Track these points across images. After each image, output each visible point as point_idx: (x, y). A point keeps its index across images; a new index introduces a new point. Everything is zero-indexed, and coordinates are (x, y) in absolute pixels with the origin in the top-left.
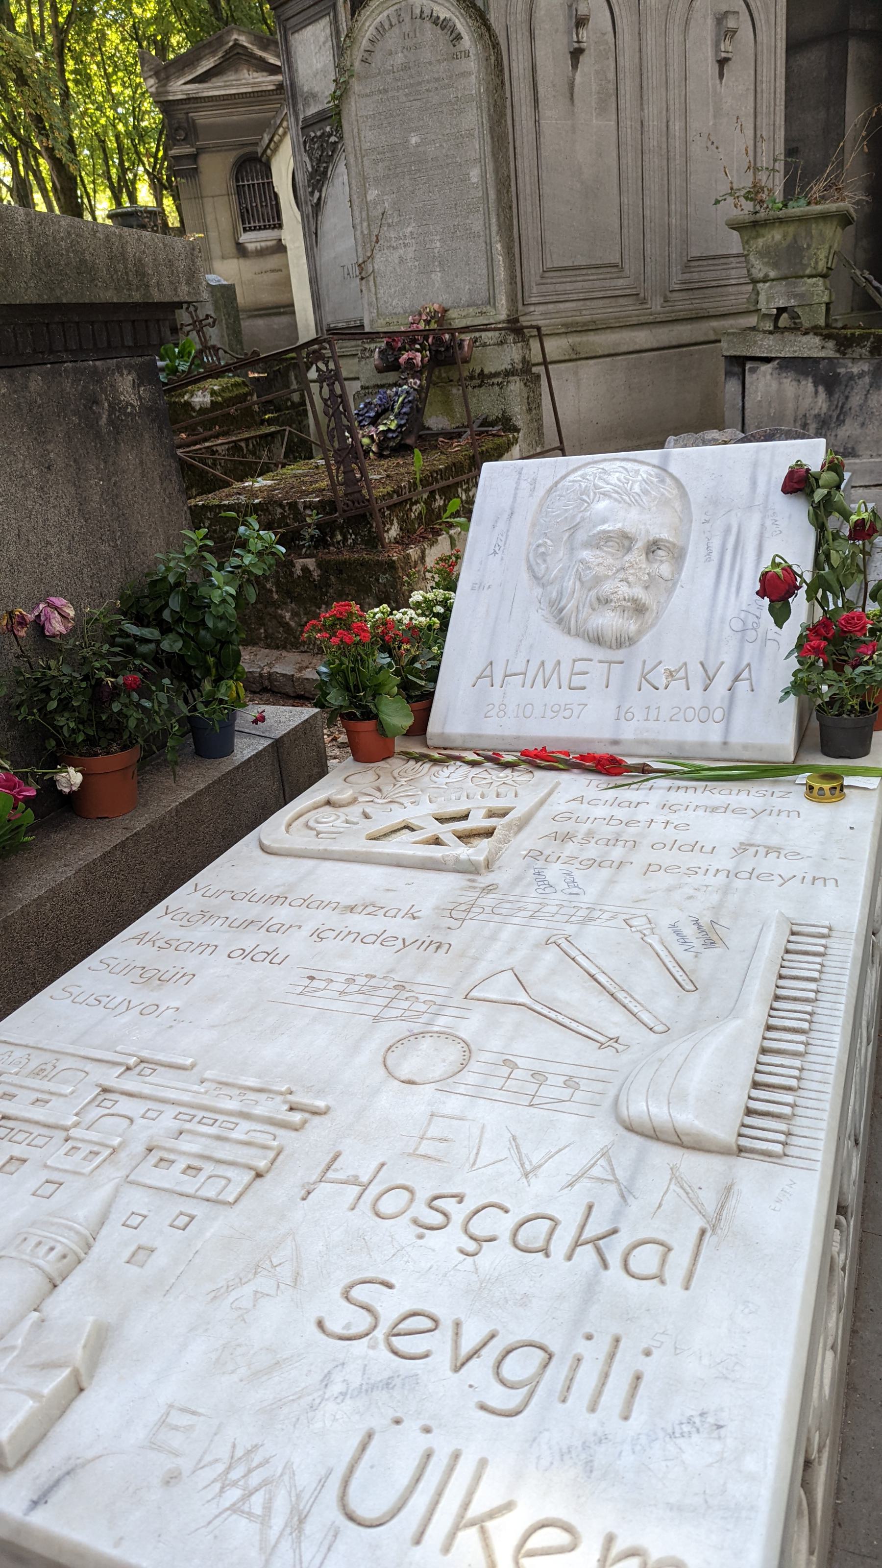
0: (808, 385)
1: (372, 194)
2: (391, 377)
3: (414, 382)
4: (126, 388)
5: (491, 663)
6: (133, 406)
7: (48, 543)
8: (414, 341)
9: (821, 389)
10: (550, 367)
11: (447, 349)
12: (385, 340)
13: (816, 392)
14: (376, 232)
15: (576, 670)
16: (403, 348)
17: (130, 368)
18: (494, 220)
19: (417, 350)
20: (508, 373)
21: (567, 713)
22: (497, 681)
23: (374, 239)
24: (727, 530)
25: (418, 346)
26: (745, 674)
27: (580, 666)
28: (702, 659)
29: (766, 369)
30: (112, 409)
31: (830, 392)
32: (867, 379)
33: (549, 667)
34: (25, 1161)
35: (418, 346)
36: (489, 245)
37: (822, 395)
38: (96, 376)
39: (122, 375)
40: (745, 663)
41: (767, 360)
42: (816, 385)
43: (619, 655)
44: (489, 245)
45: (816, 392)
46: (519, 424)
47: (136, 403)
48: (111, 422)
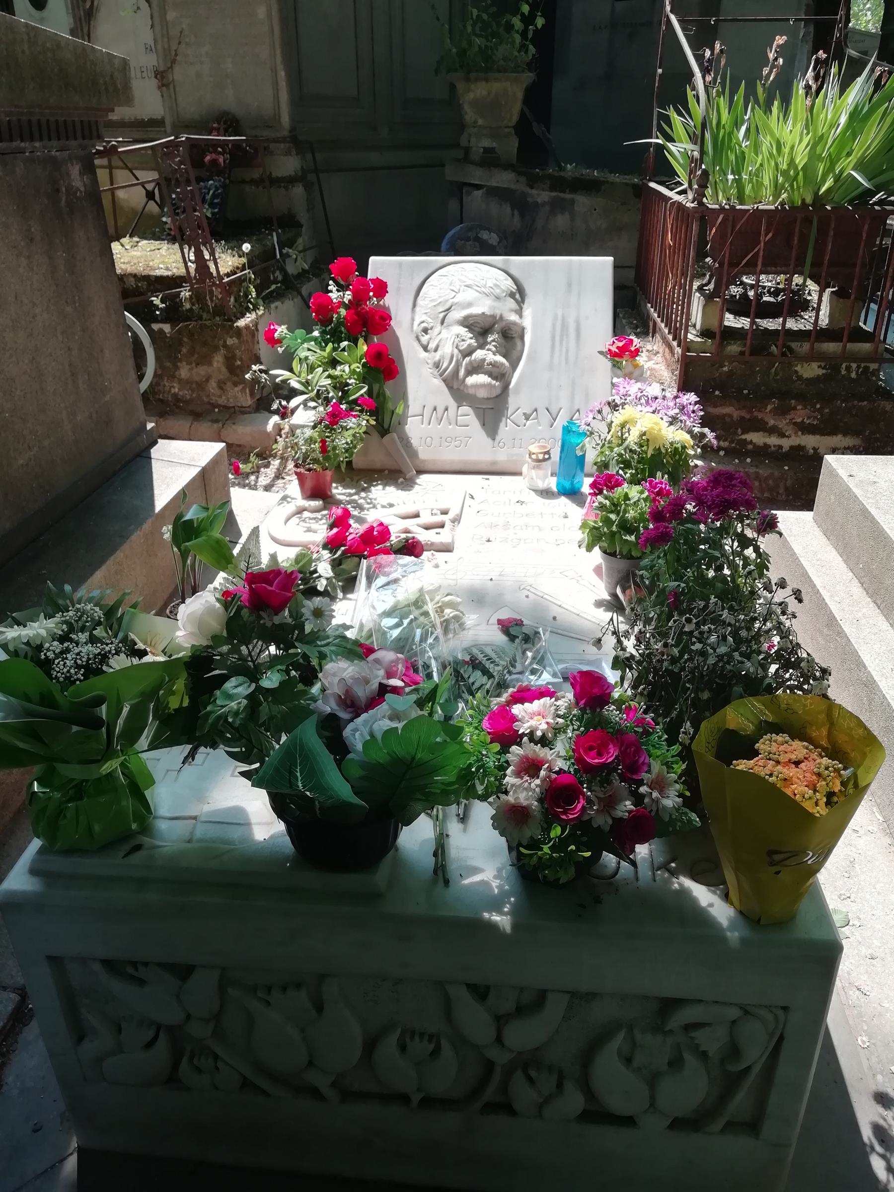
0: (507, 209)
1: (171, 15)
6: (81, 192)
9: (516, 212)
10: (321, 175)
13: (513, 215)
14: (174, 47)
18: (278, 52)
19: (220, 153)
23: (173, 53)
24: (555, 318)
25: (220, 149)
28: (547, 406)
29: (478, 193)
31: (522, 215)
32: (547, 208)
34: (159, 760)
36: (275, 71)
37: (517, 218)
40: (576, 408)
41: (478, 187)
42: (512, 209)
44: (275, 71)
45: (513, 215)
46: (303, 221)
47: (82, 189)
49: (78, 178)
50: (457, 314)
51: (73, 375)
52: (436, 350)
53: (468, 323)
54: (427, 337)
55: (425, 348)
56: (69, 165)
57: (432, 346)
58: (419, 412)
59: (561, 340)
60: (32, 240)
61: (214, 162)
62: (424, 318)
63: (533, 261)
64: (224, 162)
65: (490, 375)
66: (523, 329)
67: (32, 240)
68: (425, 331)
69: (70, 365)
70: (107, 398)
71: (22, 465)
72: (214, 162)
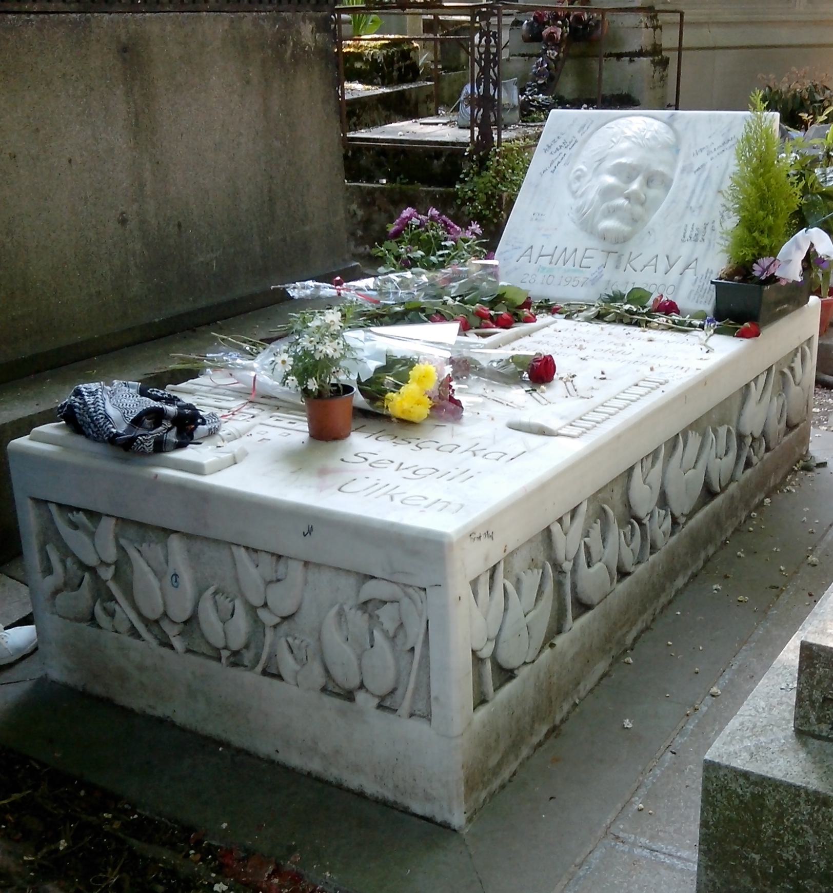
2: (536, 47)
3: (552, 53)
4: (308, 33)
5: (532, 247)
6: (310, 47)
7: (241, 134)
8: (557, 18)
10: (683, 53)
11: (585, 28)
12: (533, 14)
15: (586, 255)
16: (548, 23)
17: (311, 19)
19: (559, 26)
20: (640, 54)
21: (575, 283)
22: (533, 260)
25: (560, 22)
26: (693, 265)
27: (589, 253)
30: (295, 44)
33: (569, 252)
35: (560, 22)
38: (287, 25)
39: (305, 22)
40: (694, 258)
43: (616, 248)
48: (293, 55)
49: (309, 35)
50: (609, 164)
51: (270, 200)
52: (581, 196)
53: (618, 170)
54: (578, 184)
55: (574, 193)
56: (302, 23)
57: (579, 193)
58: (551, 252)
59: (703, 189)
60: (248, 83)
61: (551, 35)
62: (582, 167)
63: (720, 116)
64: (562, 35)
65: (621, 220)
66: (672, 180)
67: (248, 83)
68: (578, 178)
69: (270, 191)
70: (307, 228)
71: (202, 262)
72: (551, 36)
